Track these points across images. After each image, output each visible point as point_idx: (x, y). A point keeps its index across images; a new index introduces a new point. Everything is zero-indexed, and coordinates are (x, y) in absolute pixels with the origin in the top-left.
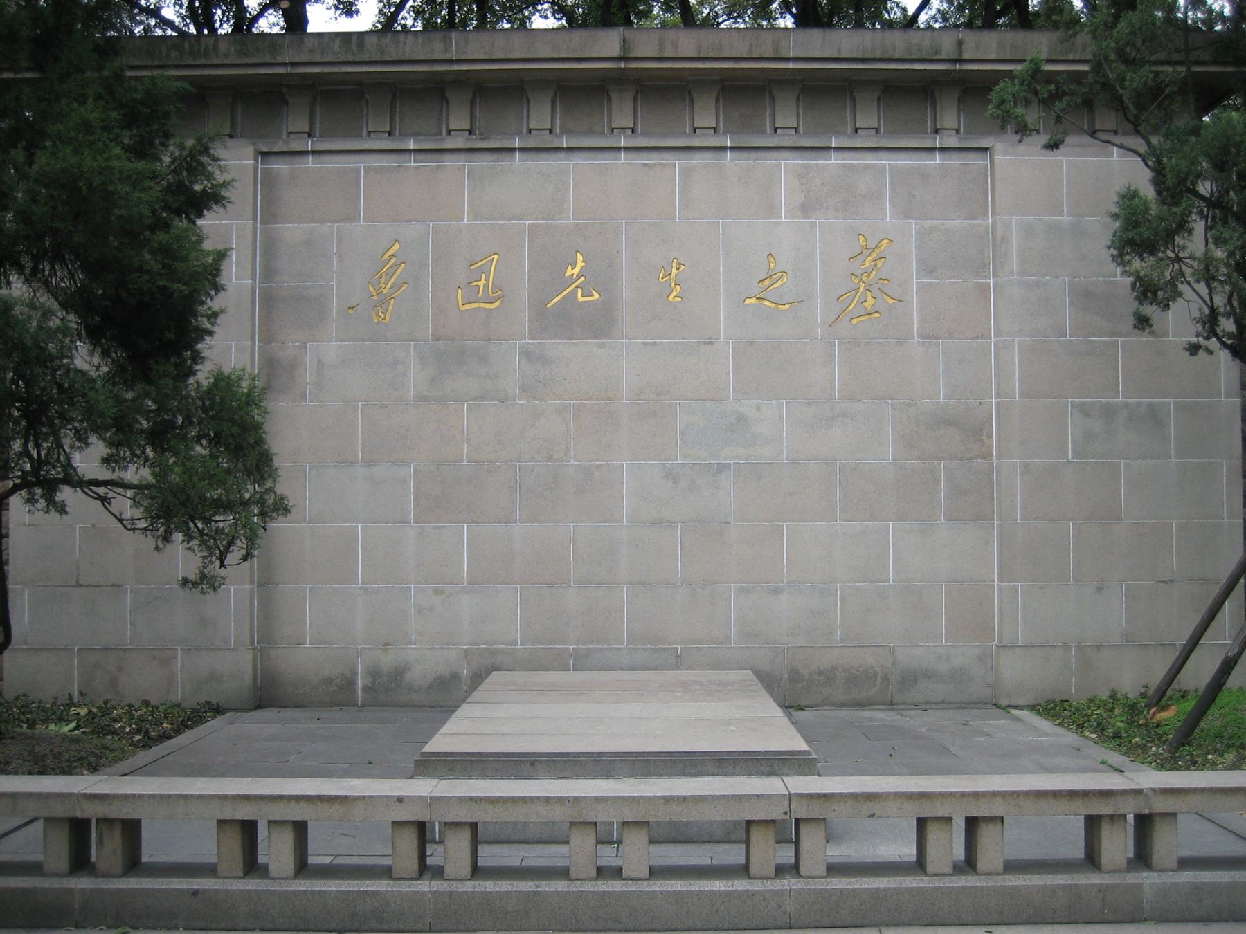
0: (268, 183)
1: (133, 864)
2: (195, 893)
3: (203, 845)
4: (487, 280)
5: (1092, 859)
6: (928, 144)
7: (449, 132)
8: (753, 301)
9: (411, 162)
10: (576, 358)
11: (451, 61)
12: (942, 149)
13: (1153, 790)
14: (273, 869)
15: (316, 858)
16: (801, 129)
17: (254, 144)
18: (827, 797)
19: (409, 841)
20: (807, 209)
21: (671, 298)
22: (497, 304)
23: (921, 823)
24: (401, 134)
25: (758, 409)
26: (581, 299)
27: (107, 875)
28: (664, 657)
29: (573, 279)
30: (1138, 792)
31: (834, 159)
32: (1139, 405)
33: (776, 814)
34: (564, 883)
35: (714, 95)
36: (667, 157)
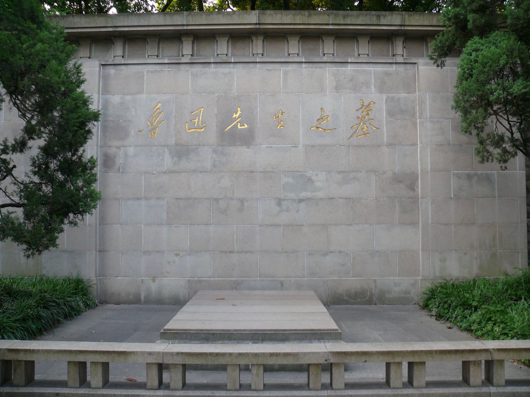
0: (105, 78)
1: (30, 381)
2: (57, 394)
3: (60, 371)
4: (199, 119)
5: (466, 381)
6: (390, 61)
7: (183, 56)
8: (314, 128)
9: (166, 68)
10: (242, 155)
11: (183, 25)
12: (396, 63)
13: (493, 349)
14: (93, 384)
15: (112, 378)
16: (405, 55)
17: (99, 61)
18: (345, 354)
19: (155, 372)
20: (337, 88)
21: (278, 127)
22: (203, 129)
23: (388, 365)
24: (162, 56)
25: (317, 175)
26: (239, 127)
27: (18, 386)
28: (279, 288)
29: (236, 119)
30: (487, 350)
31: (350, 67)
32: (482, 174)
33: (322, 361)
34: (225, 392)
35: (227, 38)
36: (277, 66)
